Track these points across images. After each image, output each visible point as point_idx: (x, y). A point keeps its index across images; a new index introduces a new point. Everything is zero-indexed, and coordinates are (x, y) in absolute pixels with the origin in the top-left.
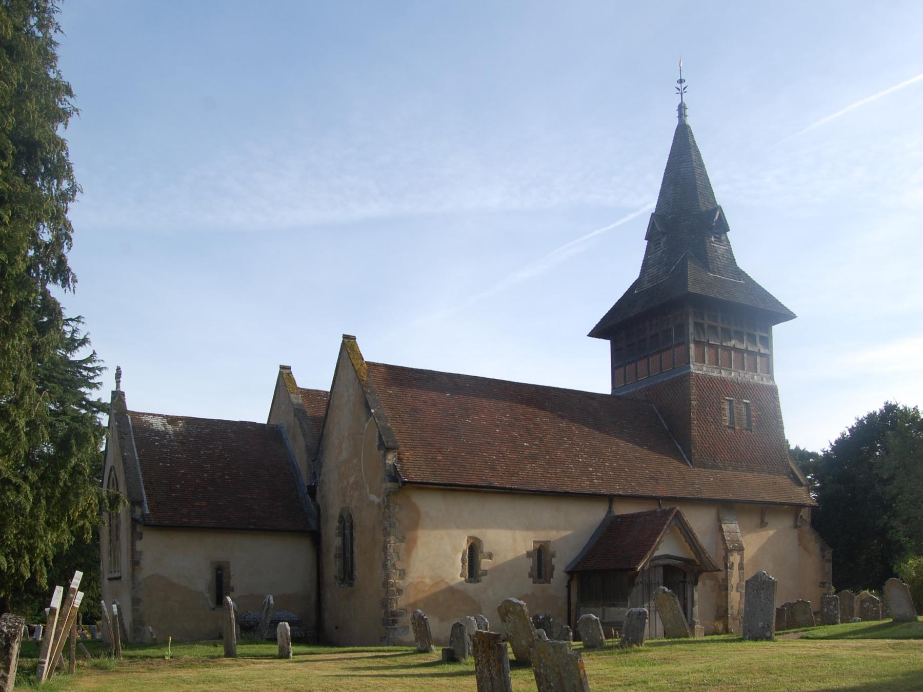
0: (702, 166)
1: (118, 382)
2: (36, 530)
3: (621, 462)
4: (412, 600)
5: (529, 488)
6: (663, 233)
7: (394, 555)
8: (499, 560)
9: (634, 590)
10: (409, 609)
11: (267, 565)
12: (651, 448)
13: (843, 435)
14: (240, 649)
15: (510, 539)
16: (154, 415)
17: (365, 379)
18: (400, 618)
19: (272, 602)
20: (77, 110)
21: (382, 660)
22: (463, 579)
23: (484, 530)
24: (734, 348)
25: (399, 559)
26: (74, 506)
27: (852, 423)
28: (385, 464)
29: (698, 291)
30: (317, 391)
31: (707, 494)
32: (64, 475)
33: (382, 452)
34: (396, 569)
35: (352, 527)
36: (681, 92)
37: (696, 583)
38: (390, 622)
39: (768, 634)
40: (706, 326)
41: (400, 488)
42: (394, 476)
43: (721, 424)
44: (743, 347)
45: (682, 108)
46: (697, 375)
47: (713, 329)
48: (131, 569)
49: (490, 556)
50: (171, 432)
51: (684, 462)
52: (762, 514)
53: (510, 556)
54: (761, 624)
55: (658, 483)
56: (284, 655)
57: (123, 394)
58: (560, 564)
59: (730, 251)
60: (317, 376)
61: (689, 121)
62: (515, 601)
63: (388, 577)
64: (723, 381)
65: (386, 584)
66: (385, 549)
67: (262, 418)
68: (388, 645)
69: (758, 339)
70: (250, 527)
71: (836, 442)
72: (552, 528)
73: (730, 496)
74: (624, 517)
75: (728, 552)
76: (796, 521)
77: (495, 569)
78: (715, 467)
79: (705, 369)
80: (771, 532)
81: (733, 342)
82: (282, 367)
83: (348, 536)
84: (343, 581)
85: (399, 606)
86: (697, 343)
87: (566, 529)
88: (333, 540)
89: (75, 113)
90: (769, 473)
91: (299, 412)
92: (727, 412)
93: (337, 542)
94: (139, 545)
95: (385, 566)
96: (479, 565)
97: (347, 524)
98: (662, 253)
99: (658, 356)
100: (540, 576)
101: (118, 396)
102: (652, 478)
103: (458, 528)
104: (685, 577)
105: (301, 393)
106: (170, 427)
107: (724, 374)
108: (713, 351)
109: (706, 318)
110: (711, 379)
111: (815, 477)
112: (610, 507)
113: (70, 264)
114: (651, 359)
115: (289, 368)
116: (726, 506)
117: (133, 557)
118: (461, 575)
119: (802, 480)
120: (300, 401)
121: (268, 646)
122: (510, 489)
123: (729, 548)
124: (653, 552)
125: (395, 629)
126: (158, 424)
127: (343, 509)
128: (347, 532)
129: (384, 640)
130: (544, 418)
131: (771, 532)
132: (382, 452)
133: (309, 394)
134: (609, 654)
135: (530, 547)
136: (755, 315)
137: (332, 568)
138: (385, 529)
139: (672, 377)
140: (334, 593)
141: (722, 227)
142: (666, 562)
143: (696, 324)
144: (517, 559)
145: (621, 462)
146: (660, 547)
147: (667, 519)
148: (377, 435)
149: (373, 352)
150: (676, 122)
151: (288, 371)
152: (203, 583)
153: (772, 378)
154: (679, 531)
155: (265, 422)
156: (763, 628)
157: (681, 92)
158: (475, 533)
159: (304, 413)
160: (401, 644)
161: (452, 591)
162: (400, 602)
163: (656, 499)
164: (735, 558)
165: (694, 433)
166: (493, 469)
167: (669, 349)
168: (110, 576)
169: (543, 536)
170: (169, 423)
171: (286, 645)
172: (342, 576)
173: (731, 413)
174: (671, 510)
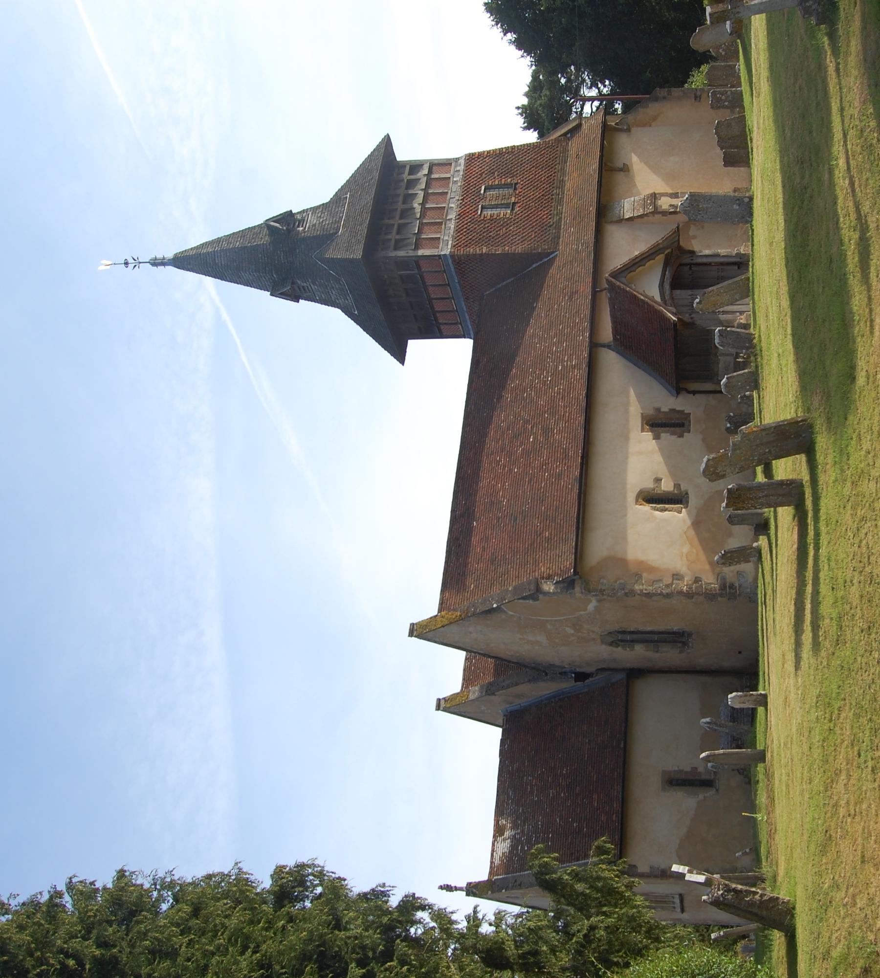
0: (218, 241)
1: (456, 889)
2: (633, 916)
3: (552, 333)
4: (707, 567)
5: (582, 437)
6: (293, 283)
7: (656, 586)
8: (662, 471)
9: (698, 322)
10: (717, 570)
11: (665, 730)
12: (536, 297)
13: (511, 42)
14: (760, 746)
15: (639, 458)
16: (493, 851)
17: (459, 613)
18: (728, 580)
19: (708, 720)
20: (236, 864)
21: (768, 597)
22: (684, 510)
23: (628, 487)
24: (423, 204)
25: (661, 580)
26: (609, 881)
27: (497, 31)
28: (554, 593)
29: (361, 247)
30: (464, 670)
31: (590, 236)
32: (580, 887)
33: (541, 596)
34: (672, 584)
35: (624, 632)
36: (138, 263)
37: (692, 253)
38: (732, 591)
39: (746, 200)
40: (398, 237)
41: (580, 578)
42: (568, 584)
43: (509, 219)
44: (421, 195)
45: (156, 263)
46: (453, 246)
47: (401, 228)
48: (671, 880)
49: (658, 480)
50: (513, 833)
51: (551, 262)
52: (614, 170)
53: (658, 458)
54: (736, 207)
55: (576, 292)
56: (763, 700)
57: (469, 884)
58: (668, 402)
59: (314, 210)
60: (448, 667)
61: (170, 255)
62: (703, 465)
63: (680, 593)
64: (460, 216)
65: (689, 595)
66: (648, 595)
67: (496, 733)
68: (757, 594)
69: (412, 177)
70: (622, 745)
71: (520, 49)
72: (627, 412)
73: (593, 209)
74: (615, 332)
75: (656, 211)
76: (621, 130)
77: (672, 474)
78: (558, 228)
79: (446, 238)
80: (635, 159)
81: (416, 205)
82: (438, 708)
83: (635, 636)
84: (685, 644)
85: (714, 581)
86: (417, 247)
87: (628, 396)
88: (637, 655)
89: (239, 865)
90: (566, 162)
91: (489, 690)
92: (495, 212)
93: (639, 649)
94: (643, 868)
95: (669, 596)
96: (668, 493)
97: (620, 637)
98: (314, 284)
99: (431, 289)
100: (681, 425)
101: (473, 890)
102: (570, 298)
103: (625, 515)
104: (686, 265)
105: (467, 687)
106: (507, 834)
107: (452, 216)
108: (426, 228)
109: (389, 237)
110: (458, 230)
111: (564, 72)
112: (604, 346)
113: (366, 889)
114: (432, 296)
115: (439, 700)
116: (604, 212)
117: (656, 877)
118: (680, 512)
119: (574, 124)
120: (477, 688)
121: (758, 725)
122: (582, 458)
123: (653, 211)
124: (656, 302)
125: (740, 586)
126: (503, 847)
127: (603, 642)
128: (628, 637)
129: (752, 599)
130: (501, 419)
131: (635, 159)
132: (541, 596)
133: (468, 678)
134: (762, 368)
135: (648, 435)
136: (386, 180)
137: (670, 655)
138: (626, 594)
139: (454, 274)
140: (699, 655)
141: (287, 218)
142: (667, 287)
143: (396, 248)
144: (661, 450)
145: (552, 333)
146: (650, 294)
147: (619, 287)
148: (521, 601)
149: (427, 603)
150: (170, 268)
151: (442, 702)
152: (687, 802)
153: (457, 160)
154: (632, 274)
155: (501, 730)
156: (739, 205)
157: (138, 263)
158: (631, 496)
159: (490, 684)
160: (756, 579)
161: (696, 524)
162: (710, 580)
163: (595, 294)
164: (665, 203)
165: (519, 249)
166: (559, 476)
167: (422, 278)
168: (679, 910)
169: (635, 421)
170: (502, 834)
171: (754, 698)
172: (680, 645)
173: (496, 207)
174: (607, 280)
